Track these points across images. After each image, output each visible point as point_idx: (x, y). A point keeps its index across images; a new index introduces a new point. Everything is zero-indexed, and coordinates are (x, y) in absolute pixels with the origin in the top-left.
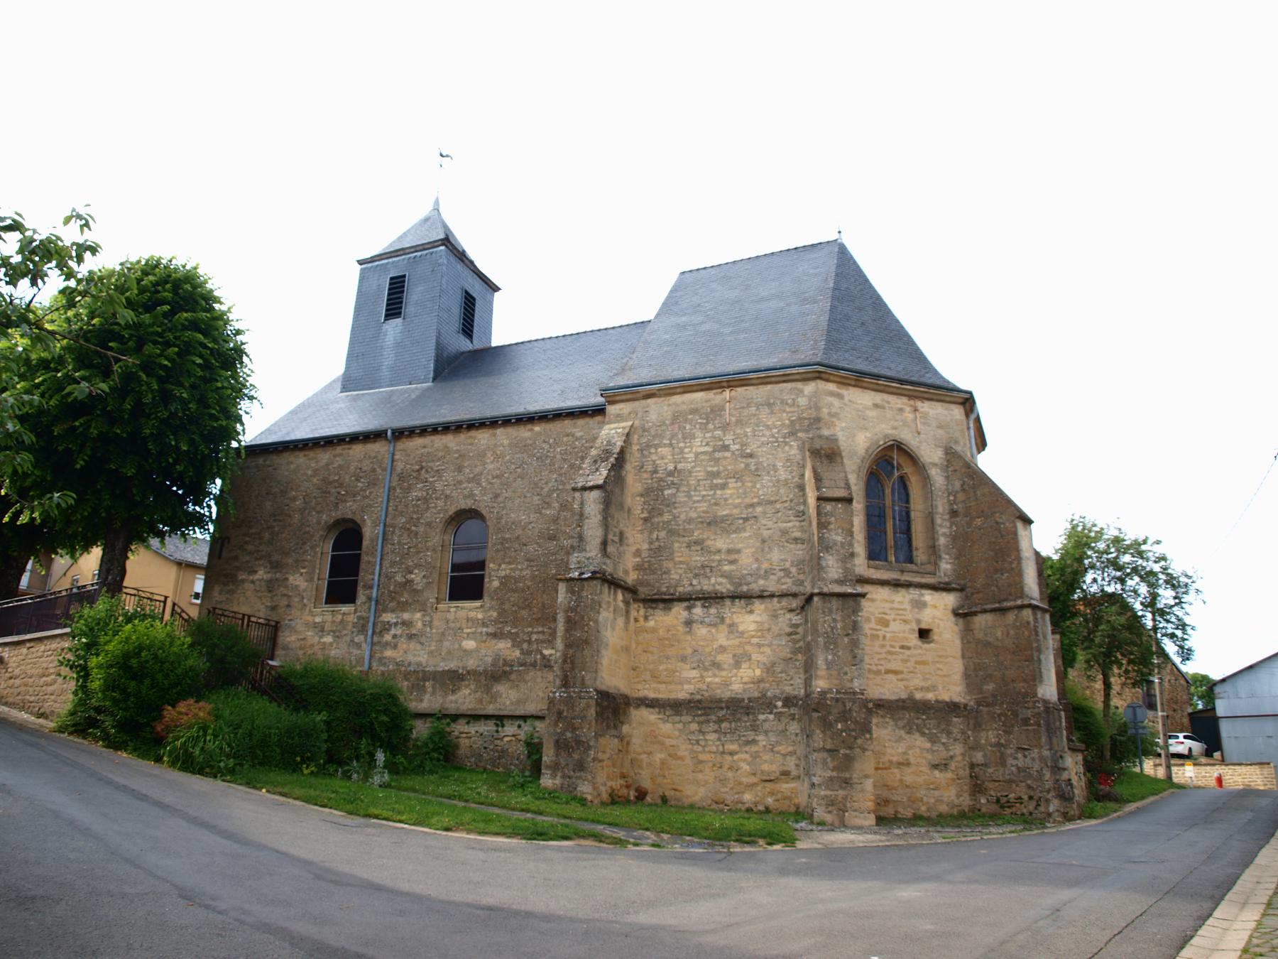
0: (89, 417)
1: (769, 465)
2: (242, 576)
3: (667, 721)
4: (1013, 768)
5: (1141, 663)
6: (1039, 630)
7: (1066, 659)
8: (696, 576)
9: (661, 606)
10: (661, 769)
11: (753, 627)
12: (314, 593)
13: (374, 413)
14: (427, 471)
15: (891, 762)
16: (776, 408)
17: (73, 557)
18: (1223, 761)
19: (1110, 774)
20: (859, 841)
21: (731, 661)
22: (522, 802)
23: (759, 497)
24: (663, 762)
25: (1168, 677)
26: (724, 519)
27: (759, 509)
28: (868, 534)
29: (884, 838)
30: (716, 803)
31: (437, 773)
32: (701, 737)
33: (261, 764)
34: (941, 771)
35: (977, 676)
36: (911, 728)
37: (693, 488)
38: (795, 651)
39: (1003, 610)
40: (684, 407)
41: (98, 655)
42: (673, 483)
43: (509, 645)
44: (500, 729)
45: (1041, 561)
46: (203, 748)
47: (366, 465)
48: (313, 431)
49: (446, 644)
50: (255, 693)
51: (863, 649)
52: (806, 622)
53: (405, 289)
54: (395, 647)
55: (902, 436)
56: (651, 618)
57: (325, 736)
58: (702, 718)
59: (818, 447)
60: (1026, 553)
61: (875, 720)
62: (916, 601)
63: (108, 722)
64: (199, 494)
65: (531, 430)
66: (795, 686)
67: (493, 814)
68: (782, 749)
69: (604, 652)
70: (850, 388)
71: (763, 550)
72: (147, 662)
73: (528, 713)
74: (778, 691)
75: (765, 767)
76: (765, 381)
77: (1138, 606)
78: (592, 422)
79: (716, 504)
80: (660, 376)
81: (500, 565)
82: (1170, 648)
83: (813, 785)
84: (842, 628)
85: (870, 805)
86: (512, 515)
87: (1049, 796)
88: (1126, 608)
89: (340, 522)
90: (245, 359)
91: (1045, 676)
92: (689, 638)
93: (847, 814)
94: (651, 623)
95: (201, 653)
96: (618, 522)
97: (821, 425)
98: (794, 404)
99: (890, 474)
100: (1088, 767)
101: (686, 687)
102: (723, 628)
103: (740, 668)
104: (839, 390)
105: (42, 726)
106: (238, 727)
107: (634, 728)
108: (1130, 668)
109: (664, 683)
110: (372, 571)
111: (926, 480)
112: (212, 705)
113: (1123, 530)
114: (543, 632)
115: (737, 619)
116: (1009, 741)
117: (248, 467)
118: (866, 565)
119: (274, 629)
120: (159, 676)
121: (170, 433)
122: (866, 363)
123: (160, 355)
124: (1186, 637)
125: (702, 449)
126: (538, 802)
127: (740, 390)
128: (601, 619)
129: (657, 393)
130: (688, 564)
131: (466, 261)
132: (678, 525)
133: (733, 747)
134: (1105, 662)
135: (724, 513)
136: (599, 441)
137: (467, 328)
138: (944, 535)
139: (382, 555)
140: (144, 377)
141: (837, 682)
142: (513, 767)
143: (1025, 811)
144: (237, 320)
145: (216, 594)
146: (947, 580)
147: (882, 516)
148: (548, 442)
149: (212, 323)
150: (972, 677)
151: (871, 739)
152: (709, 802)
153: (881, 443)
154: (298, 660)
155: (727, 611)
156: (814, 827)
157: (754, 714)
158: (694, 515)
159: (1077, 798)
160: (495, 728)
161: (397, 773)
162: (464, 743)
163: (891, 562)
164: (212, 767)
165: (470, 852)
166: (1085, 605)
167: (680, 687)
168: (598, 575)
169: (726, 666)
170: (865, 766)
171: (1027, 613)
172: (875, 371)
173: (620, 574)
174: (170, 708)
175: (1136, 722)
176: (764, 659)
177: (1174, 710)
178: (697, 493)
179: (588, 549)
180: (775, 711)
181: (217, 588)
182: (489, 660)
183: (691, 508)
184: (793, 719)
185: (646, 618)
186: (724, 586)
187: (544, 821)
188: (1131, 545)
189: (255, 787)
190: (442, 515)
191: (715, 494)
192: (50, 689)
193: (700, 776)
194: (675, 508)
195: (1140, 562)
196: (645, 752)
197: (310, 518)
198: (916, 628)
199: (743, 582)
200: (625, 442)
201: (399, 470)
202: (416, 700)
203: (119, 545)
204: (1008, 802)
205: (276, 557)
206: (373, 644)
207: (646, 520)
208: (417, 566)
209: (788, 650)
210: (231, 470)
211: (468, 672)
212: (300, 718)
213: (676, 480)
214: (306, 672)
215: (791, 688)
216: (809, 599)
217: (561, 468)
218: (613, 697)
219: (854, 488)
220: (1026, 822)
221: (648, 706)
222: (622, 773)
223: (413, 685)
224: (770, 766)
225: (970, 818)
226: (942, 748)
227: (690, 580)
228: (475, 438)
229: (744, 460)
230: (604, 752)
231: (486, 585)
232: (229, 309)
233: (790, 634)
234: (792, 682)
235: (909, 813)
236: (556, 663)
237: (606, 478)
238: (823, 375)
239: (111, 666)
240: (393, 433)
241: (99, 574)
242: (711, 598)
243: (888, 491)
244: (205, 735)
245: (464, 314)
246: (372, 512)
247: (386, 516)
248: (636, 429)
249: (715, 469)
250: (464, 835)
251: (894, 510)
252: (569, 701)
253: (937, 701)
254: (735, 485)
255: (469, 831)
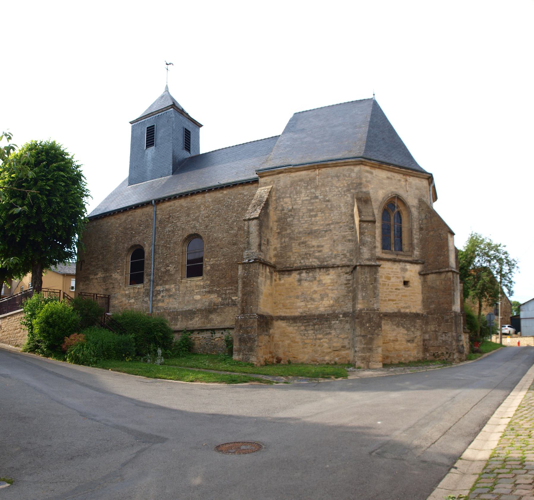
0: (18, 219)
1: (337, 205)
2: (92, 277)
3: (290, 326)
4: (441, 341)
5: (494, 297)
6: (455, 281)
7: (465, 294)
8: (303, 258)
9: (287, 273)
10: (288, 348)
11: (329, 281)
12: (124, 280)
13: (145, 193)
14: (172, 217)
15: (390, 340)
16: (341, 178)
17: (20, 278)
18: (521, 336)
19: (479, 342)
20: (375, 375)
21: (319, 297)
22: (224, 367)
23: (332, 221)
24: (289, 345)
25: (504, 302)
26: (315, 231)
27: (332, 226)
28: (383, 238)
29: (386, 373)
30: (313, 361)
31: (185, 357)
32: (306, 333)
33: (107, 358)
34: (411, 343)
35: (428, 301)
36: (399, 325)
37: (301, 217)
38: (348, 292)
39: (440, 273)
40: (296, 179)
41: (35, 319)
42: (291, 215)
43: (216, 296)
44: (213, 335)
45: (457, 251)
46: (82, 354)
47: (144, 218)
48: (117, 206)
49: (187, 298)
50: (102, 328)
51: (379, 290)
52: (354, 278)
53: (155, 135)
54: (163, 301)
55: (400, 193)
56: (282, 279)
57: (134, 344)
58: (306, 324)
59: (360, 197)
60: (451, 248)
61: (383, 322)
62: (403, 268)
63: (43, 346)
64: (69, 243)
65: (222, 193)
66: (348, 307)
67: (212, 373)
68: (342, 336)
69: (261, 297)
70: (376, 169)
71: (334, 245)
72: (56, 319)
73: (226, 327)
74: (340, 310)
75: (335, 344)
76: (336, 165)
77: (495, 273)
78: (252, 187)
79: (312, 224)
80: (286, 162)
81: (210, 259)
82: (505, 290)
83: (356, 351)
84: (369, 281)
85: (380, 359)
86: (215, 235)
87: (455, 352)
88: (491, 273)
89: (132, 247)
90: (82, 178)
91: (455, 301)
92: (300, 287)
93: (370, 363)
94: (282, 282)
95: (78, 313)
96: (266, 234)
97: (362, 186)
98: (349, 176)
99: (393, 210)
100: (471, 339)
101: (299, 310)
102: (316, 282)
103: (323, 300)
104: (371, 170)
105: (17, 350)
106: (97, 343)
107: (275, 330)
108: (490, 298)
109: (289, 309)
110: (150, 267)
111: (409, 213)
112: (85, 335)
113: (492, 240)
114: (232, 289)
115: (322, 278)
116: (439, 330)
117: (89, 227)
118: (381, 252)
119: (108, 298)
120: (61, 325)
121: (53, 218)
122: (384, 157)
123: (45, 185)
124: (511, 286)
125: (305, 198)
126: (232, 367)
127: (324, 170)
128: (259, 281)
129: (284, 171)
130: (299, 253)
131: (184, 114)
132: (294, 235)
133: (320, 336)
134: (480, 295)
135: (316, 228)
136: (256, 196)
137: (187, 147)
138: (416, 238)
139: (154, 260)
140: (40, 196)
141: (366, 305)
142: (220, 352)
143: (444, 358)
144: (76, 161)
145: (81, 287)
146: (417, 259)
147: (389, 230)
148: (231, 198)
149: (66, 165)
150: (426, 302)
151: (381, 330)
152: (310, 361)
153: (390, 195)
154: (120, 312)
155: (317, 274)
156: (356, 370)
157: (330, 321)
158: (301, 230)
159: (465, 352)
160: (211, 335)
161: (168, 358)
162: (197, 342)
163: (392, 251)
164: (87, 361)
165: (202, 390)
166: (474, 271)
167: (296, 310)
168: (257, 261)
169: (317, 300)
170: (379, 342)
171: (450, 274)
172: (388, 161)
173: (268, 259)
174: (67, 338)
175: (490, 321)
176: (334, 296)
177: (505, 316)
178: (303, 219)
179: (252, 248)
180: (339, 319)
181: (81, 284)
182: (207, 303)
183: (300, 227)
184: (347, 323)
185: (280, 279)
186: (315, 263)
187: (235, 375)
188: (494, 247)
189: (106, 369)
190: (181, 238)
191: (311, 219)
192: (19, 335)
193: (306, 350)
194: (293, 227)
195: (497, 254)
196: (281, 341)
197: (120, 247)
198: (402, 280)
199: (325, 260)
200: (268, 196)
201: (159, 219)
202: (174, 325)
203: (38, 271)
204: (438, 355)
205: (106, 266)
206: (153, 301)
207: (279, 233)
208: (171, 263)
209: (345, 292)
210: (83, 229)
211: (198, 310)
212: (123, 337)
213: (293, 214)
214: (124, 317)
215: (346, 308)
216: (355, 268)
217: (238, 210)
218: (266, 317)
219: (376, 216)
220: (445, 363)
221: (281, 320)
222: (270, 351)
223: (172, 318)
224: (337, 344)
225: (422, 363)
226: (412, 333)
227: (300, 261)
228: (195, 199)
229: (325, 203)
230: (262, 342)
231: (204, 269)
232: (72, 157)
233: (346, 284)
234: (347, 306)
235: (396, 362)
236: (238, 303)
237: (260, 214)
238: (364, 163)
239: (41, 323)
240: (155, 202)
241: (32, 284)
242: (310, 269)
243: (392, 218)
244: (83, 348)
245: (185, 134)
246: (148, 240)
247: (155, 241)
248: (274, 189)
249: (311, 208)
250: (199, 383)
251: (394, 227)
252: (245, 320)
253: (410, 313)
254: (321, 215)
255: (201, 382)
